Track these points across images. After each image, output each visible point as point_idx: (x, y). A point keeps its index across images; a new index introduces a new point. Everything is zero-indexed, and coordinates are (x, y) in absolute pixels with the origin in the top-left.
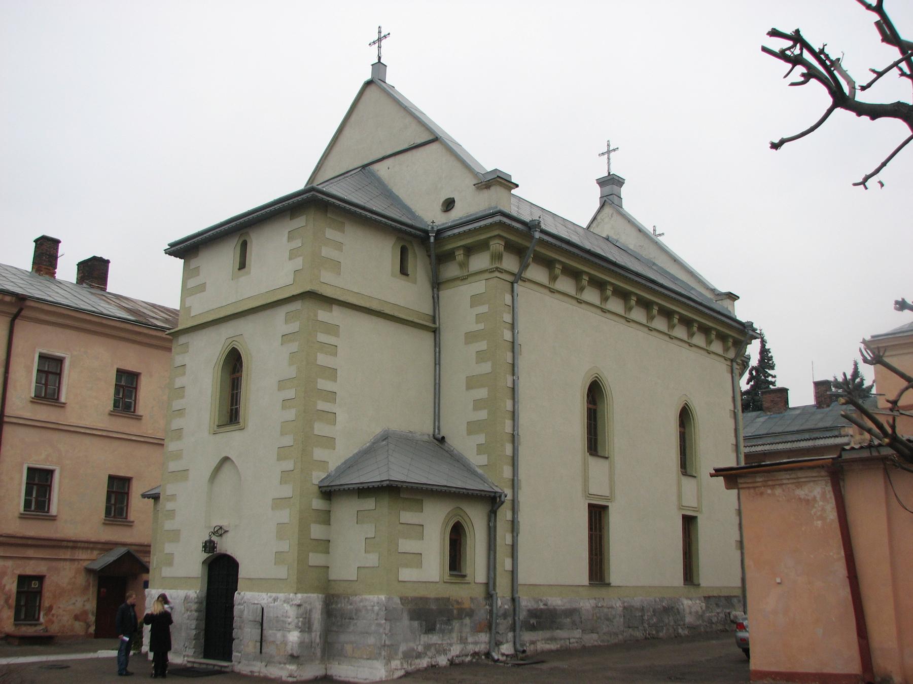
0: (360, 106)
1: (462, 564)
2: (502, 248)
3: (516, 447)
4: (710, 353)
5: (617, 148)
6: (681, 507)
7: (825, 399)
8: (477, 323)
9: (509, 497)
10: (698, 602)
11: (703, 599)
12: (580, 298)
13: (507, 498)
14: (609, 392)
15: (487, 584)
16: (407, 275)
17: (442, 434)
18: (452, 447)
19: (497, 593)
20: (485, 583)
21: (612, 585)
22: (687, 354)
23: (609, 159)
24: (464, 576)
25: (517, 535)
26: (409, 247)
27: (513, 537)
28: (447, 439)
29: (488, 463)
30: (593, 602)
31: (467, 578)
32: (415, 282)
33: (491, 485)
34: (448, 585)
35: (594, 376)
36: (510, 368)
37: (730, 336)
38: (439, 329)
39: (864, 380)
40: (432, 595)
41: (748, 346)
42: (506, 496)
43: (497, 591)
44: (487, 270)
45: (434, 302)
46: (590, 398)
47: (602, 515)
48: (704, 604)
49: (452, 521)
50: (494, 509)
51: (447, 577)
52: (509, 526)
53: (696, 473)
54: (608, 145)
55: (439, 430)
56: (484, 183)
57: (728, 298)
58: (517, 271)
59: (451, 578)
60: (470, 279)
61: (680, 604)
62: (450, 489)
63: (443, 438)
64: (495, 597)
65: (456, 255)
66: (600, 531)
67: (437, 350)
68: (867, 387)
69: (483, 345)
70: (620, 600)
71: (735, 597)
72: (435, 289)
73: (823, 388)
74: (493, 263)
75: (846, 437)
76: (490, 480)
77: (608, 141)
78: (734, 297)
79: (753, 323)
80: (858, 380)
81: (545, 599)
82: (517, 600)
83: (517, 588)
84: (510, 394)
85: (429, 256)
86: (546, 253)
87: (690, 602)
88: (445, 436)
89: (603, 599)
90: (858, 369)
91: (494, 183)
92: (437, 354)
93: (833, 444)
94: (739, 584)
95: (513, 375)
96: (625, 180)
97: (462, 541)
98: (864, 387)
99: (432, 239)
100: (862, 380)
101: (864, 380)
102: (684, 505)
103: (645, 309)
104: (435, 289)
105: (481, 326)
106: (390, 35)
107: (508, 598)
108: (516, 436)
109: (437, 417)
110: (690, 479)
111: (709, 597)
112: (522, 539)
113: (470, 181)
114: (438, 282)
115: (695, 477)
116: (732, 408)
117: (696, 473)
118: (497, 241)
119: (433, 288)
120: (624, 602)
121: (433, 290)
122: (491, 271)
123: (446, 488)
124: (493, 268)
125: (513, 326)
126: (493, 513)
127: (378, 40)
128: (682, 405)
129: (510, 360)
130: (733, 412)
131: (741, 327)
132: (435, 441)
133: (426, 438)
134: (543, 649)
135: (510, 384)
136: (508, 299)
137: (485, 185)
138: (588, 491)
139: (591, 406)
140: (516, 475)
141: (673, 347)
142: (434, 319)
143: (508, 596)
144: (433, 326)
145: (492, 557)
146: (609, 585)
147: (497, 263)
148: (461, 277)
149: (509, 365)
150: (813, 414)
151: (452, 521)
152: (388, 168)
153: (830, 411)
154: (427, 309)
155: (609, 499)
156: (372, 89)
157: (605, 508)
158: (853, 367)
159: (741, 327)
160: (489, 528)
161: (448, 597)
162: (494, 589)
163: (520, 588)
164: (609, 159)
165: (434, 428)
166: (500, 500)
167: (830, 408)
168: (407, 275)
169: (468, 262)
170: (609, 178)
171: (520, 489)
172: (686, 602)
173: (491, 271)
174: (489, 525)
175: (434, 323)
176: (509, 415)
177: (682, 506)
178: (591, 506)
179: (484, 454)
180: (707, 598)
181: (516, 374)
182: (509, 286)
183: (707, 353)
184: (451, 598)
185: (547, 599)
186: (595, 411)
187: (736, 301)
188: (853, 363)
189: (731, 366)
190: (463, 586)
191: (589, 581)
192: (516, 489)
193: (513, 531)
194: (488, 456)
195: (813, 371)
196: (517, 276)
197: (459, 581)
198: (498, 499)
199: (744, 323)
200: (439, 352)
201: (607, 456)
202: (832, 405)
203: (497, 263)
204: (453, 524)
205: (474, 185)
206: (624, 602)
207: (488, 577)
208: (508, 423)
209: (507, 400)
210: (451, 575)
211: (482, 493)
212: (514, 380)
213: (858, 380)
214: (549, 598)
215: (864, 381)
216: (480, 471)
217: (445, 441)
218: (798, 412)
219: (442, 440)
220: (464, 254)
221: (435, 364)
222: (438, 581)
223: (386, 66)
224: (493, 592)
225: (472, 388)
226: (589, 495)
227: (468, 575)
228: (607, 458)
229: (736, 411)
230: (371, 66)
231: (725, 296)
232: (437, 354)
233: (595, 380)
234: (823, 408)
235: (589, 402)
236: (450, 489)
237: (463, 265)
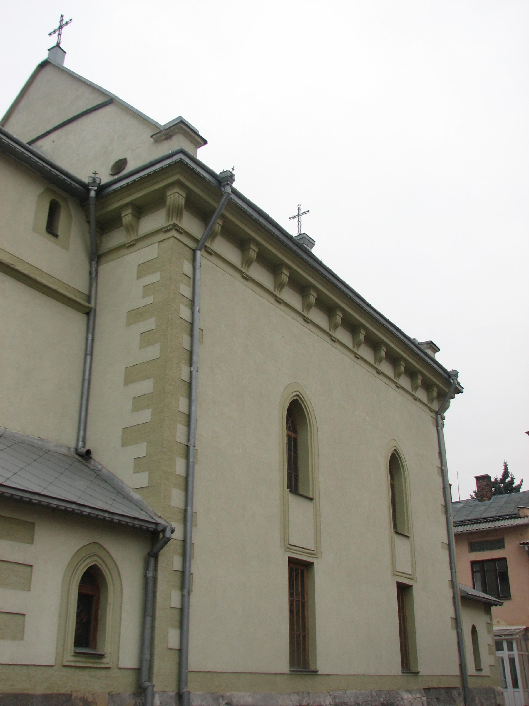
0: (32, 90)
1: (99, 635)
2: (182, 201)
3: (191, 464)
4: (416, 400)
5: (308, 211)
6: (396, 573)
7: (486, 492)
8: (144, 297)
9: (178, 535)
10: (418, 695)
11: (423, 691)
12: (279, 296)
13: (173, 536)
14: (314, 418)
15: (138, 671)
16: (56, 236)
17: (88, 447)
18: (100, 465)
19: (154, 686)
20: (135, 669)
21: (319, 673)
22: (392, 392)
23: (299, 221)
24: (101, 656)
25: (189, 594)
26: (62, 204)
27: (183, 596)
28: (94, 456)
29: (148, 484)
30: (295, 698)
31: (104, 660)
32: (66, 247)
33: (152, 515)
34: (71, 671)
35: (293, 395)
36: (186, 356)
37: (436, 384)
38: (95, 310)
39: (514, 479)
40: (40, 690)
41: (452, 400)
42: (173, 532)
43: (155, 681)
44: (162, 229)
45: (91, 278)
46: (289, 423)
47: (305, 575)
48: (424, 699)
49: (85, 564)
50: (155, 550)
51: (69, 658)
52: (176, 579)
53: (408, 533)
54: (299, 209)
55: (84, 441)
56: (164, 132)
57: (429, 348)
58: (200, 237)
59: (78, 659)
60: (139, 245)
61: (400, 699)
62: (82, 509)
63: (88, 452)
64: (149, 691)
65: (122, 215)
66: (303, 597)
67: (90, 336)
68: (516, 486)
69: (150, 324)
70: (330, 695)
71: (454, 688)
72: (94, 263)
73: (484, 483)
74: (170, 219)
75: (526, 518)
76: (151, 509)
77: (299, 205)
78: (435, 347)
79: (458, 373)
80: (509, 479)
81: (228, 694)
82: (185, 697)
83: (187, 676)
84: (184, 390)
85: (88, 222)
86: (239, 224)
87: (410, 696)
88: (92, 451)
89: (309, 693)
90: (508, 469)
91: (177, 131)
92: (90, 341)
93: (514, 525)
94: (457, 672)
95: (191, 365)
96: (315, 242)
97: (101, 596)
98: (514, 486)
99: (93, 194)
100: (513, 479)
101: (514, 479)
102: (397, 570)
103: (351, 333)
104: (94, 263)
105: (150, 300)
106: (72, 21)
107: (172, 694)
108: (192, 448)
109: (82, 425)
110: (404, 540)
111: (429, 689)
112: (194, 600)
113: (146, 135)
114: (99, 253)
115: (408, 537)
116: (439, 465)
117: (408, 533)
118: (176, 190)
119: (91, 260)
120: (335, 698)
121: (91, 264)
122: (166, 230)
123: (74, 506)
124: (169, 226)
125: (192, 303)
126: (153, 557)
127: (59, 28)
128: (392, 450)
129: (187, 347)
130: (440, 468)
131: (446, 376)
132: (78, 457)
133: (65, 451)
134: (170, 140)
135: (185, 376)
136: (187, 268)
137: (166, 134)
138: (289, 541)
139: (291, 434)
140: (189, 504)
141: (380, 383)
142: (89, 299)
143: (172, 690)
144: (87, 304)
145: (148, 626)
146: (315, 672)
147: (174, 218)
148: (128, 243)
149: (188, 351)
150: (476, 506)
151: (85, 564)
152: (53, 142)
153: (492, 503)
154: (84, 289)
155: (315, 555)
156: (47, 71)
157: (309, 565)
158: (503, 467)
159: (446, 376)
160: (146, 578)
161: (69, 692)
162: (150, 679)
163: (190, 676)
164: (299, 221)
165: (78, 440)
166: (164, 536)
167: (491, 501)
168: (56, 236)
169: (138, 225)
170: (300, 237)
171: (196, 526)
172: (406, 696)
173: (166, 230)
174: (145, 576)
175: (89, 301)
176: (183, 419)
177: (396, 571)
178: (292, 561)
179: (143, 471)
180: (427, 690)
181: (195, 365)
182: (189, 253)
183: (413, 399)
184: (74, 694)
185: (232, 695)
186: (295, 440)
187: (437, 353)
188: (503, 464)
189: (436, 419)
190: (98, 673)
191: (290, 668)
192: (189, 524)
193: (182, 587)
194: (150, 473)
195: (458, 477)
196: (201, 243)
197: (90, 665)
198: (161, 535)
199: (449, 372)
200: (93, 340)
201: (311, 496)
202: (492, 498)
203: (174, 218)
204: (85, 570)
205: (151, 137)
206: (335, 698)
207: (141, 660)
208: (181, 429)
209: (181, 398)
210: (77, 654)
211: (136, 522)
212: (191, 372)
213: (509, 479)
214: (235, 693)
215: (514, 480)
216: (136, 496)
217: (91, 458)
218: (461, 505)
219: (87, 456)
220: (132, 213)
221: (86, 355)
222: (52, 663)
223: (65, 52)
224: (147, 684)
225: (133, 382)
226: (289, 546)
227: (108, 655)
228: (311, 499)
229: (443, 468)
230: (48, 52)
231: (426, 346)
232: (90, 341)
233: (296, 399)
234: (485, 500)
235: (289, 429)
236: (82, 509)
237: (131, 228)
